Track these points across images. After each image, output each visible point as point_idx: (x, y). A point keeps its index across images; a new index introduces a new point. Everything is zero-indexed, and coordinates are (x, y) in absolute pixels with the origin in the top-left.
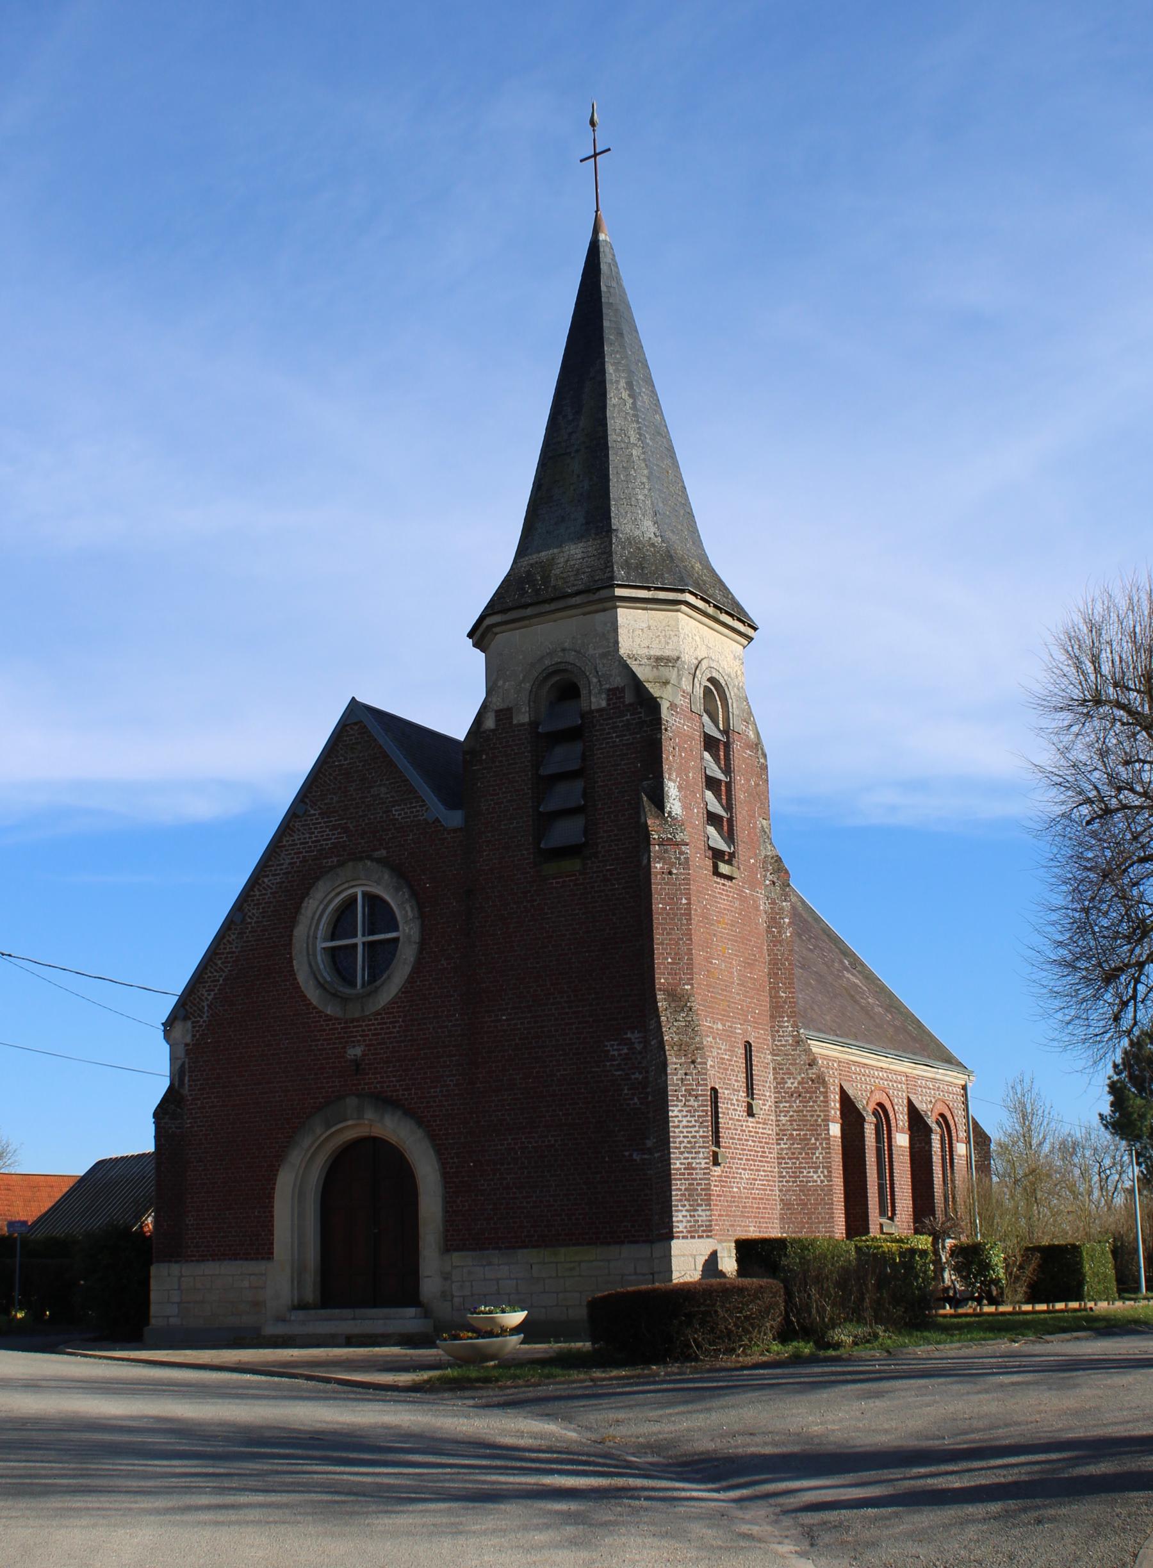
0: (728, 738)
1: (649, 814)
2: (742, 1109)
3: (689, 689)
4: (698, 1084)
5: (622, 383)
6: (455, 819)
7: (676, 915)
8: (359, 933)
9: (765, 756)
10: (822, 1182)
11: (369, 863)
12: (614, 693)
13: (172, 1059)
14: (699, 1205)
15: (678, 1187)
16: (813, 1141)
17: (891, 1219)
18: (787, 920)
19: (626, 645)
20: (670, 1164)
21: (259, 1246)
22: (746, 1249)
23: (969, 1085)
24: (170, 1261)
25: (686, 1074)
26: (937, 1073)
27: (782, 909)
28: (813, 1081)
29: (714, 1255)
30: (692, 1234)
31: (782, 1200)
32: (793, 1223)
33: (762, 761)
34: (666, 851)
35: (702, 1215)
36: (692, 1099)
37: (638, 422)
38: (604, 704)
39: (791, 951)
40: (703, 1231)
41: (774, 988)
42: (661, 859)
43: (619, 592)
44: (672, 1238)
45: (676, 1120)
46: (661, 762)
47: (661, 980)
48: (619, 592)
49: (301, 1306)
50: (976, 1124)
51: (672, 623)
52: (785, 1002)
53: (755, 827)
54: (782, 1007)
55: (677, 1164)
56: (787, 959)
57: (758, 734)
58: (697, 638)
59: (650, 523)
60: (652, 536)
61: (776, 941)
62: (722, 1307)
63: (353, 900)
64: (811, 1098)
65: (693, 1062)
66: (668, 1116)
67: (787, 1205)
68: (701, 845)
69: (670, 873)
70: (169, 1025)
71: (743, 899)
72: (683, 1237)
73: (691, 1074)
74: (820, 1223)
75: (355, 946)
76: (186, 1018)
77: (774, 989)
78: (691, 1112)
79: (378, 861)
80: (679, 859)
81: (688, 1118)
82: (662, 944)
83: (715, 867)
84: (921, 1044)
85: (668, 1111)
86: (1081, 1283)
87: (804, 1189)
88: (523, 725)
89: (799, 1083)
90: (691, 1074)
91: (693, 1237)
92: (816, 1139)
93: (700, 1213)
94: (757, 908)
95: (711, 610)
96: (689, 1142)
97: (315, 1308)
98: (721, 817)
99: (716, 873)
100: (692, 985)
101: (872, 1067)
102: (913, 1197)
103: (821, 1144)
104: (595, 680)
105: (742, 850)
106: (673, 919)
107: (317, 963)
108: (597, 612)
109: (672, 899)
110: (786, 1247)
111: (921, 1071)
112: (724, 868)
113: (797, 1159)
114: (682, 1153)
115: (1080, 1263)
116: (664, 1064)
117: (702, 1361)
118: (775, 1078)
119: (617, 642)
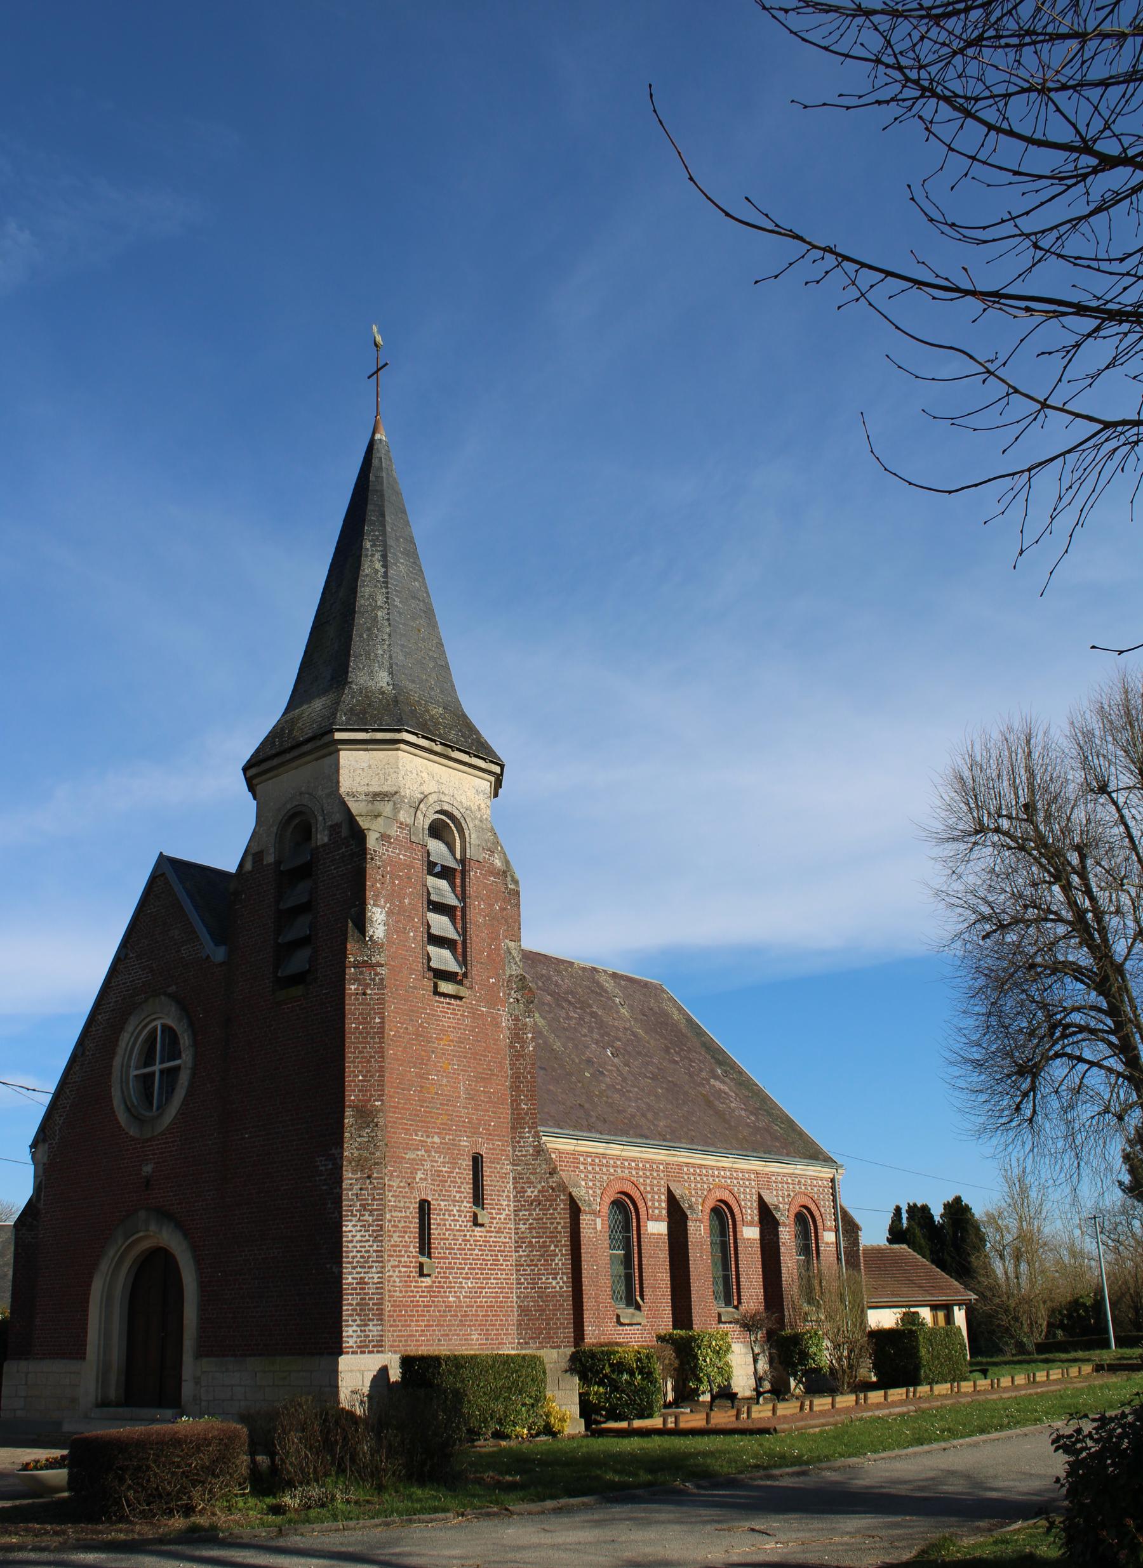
0: (464, 866)
1: (350, 939)
2: (465, 1221)
3: (410, 821)
4: (374, 1199)
5: (378, 556)
6: (219, 954)
7: (368, 1033)
9: (516, 882)
10: (561, 1288)
11: (163, 998)
12: (334, 829)
13: (35, 1177)
14: (370, 1320)
15: (350, 1301)
16: (552, 1248)
18: (530, 1035)
19: (347, 783)
21: (78, 1353)
22: (407, 1362)
23: (837, 1177)
24: (20, 1359)
25: (361, 1189)
27: (525, 1024)
28: (553, 1189)
29: (384, 1370)
30: (363, 1348)
31: (519, 1306)
32: (531, 1329)
33: (513, 887)
34: (361, 973)
35: (373, 1330)
36: (367, 1213)
37: (387, 588)
38: (326, 840)
39: (533, 1064)
40: (374, 1346)
43: (338, 736)
44: (341, 1353)
45: (350, 1234)
46: (365, 890)
47: (351, 1097)
48: (338, 736)
49: (103, 1404)
50: (845, 1214)
51: (392, 761)
52: (526, 1114)
53: (498, 948)
54: (523, 1118)
55: (349, 1279)
56: (529, 1073)
57: (507, 863)
58: (425, 775)
59: (386, 674)
60: (385, 685)
61: (518, 1056)
62: (155, 1461)
63: (155, 1029)
64: (551, 1206)
65: (369, 1177)
66: (341, 1232)
67: (524, 1311)
68: (419, 966)
69: (364, 994)
70: (34, 1145)
71: (474, 1014)
72: (353, 1353)
73: (367, 1189)
74: (558, 1328)
75: (153, 1074)
76: (44, 1141)
77: (516, 1102)
78: (365, 1226)
79: (169, 995)
80: (374, 980)
83: (436, 986)
84: (790, 1142)
85: (341, 1226)
86: (917, 1368)
87: (542, 1295)
88: (270, 865)
90: (367, 1189)
91: (363, 1352)
92: (556, 1246)
93: (371, 1327)
95: (438, 748)
96: (362, 1257)
97: (118, 1405)
98: (456, 941)
99: (436, 992)
100: (382, 1101)
102: (764, 1286)
104: (320, 818)
105: (475, 971)
106: (365, 1038)
107: (128, 1089)
108: (324, 756)
109: (365, 1020)
110: (440, 1364)
111: (772, 1167)
112: (446, 987)
113: (536, 1265)
115: (916, 1349)
116: (339, 1180)
117: (131, 1522)
118: (515, 1188)
119: (338, 782)
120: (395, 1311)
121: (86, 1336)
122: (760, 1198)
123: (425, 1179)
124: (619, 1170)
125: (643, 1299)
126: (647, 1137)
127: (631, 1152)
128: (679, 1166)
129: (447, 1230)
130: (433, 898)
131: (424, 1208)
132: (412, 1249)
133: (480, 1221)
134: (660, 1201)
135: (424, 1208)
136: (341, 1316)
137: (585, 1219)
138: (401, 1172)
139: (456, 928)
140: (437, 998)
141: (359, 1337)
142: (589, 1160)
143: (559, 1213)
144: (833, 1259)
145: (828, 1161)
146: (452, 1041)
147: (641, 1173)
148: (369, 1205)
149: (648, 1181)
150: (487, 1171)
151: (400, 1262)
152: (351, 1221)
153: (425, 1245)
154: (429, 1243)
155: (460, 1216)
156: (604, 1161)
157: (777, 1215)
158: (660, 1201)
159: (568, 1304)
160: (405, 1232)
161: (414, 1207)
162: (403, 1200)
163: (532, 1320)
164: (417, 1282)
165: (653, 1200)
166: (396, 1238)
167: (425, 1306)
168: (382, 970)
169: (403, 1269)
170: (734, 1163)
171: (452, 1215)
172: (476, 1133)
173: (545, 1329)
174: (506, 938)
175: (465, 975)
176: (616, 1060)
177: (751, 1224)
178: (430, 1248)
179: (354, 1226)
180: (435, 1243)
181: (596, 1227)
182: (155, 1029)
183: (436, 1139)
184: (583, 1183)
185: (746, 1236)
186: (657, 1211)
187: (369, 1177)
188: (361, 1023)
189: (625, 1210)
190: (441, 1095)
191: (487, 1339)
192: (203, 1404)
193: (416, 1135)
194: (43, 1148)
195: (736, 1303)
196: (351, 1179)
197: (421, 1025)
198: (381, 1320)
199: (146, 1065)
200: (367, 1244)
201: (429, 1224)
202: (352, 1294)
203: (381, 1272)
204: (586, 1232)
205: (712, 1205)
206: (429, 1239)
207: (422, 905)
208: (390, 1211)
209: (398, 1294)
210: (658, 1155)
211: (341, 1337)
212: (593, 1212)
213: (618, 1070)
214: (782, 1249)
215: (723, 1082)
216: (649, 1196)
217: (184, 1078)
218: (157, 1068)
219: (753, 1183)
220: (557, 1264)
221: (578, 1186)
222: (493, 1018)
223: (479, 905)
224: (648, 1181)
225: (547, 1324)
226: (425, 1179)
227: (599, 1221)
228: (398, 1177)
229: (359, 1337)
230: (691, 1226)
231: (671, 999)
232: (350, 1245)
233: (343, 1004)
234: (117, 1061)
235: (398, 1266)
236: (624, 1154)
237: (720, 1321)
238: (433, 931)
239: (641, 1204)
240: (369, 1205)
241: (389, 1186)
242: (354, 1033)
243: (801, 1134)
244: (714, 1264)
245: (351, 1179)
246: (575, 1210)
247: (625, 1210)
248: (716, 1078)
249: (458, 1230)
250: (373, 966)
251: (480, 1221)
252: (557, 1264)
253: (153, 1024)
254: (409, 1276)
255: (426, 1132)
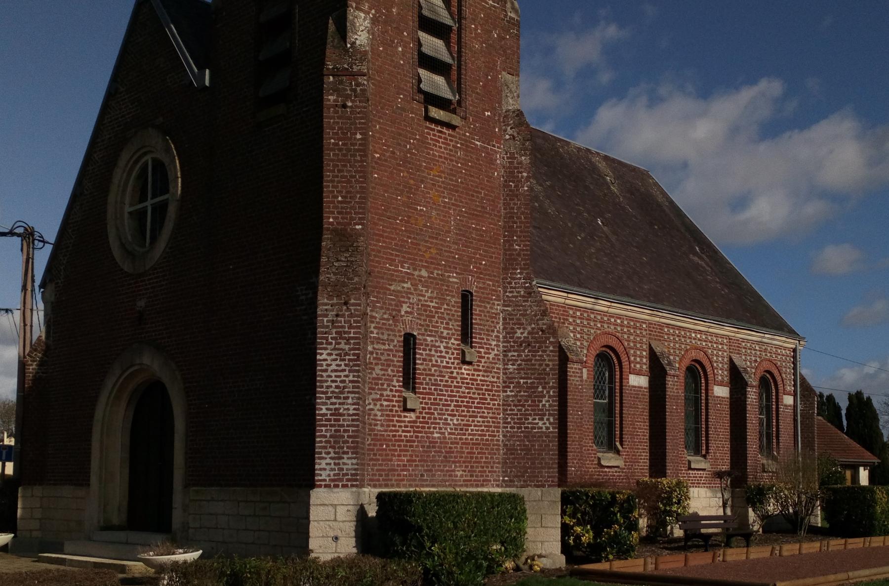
2: (451, 359)
4: (350, 327)
7: (349, 150)
8: (150, 196)
10: (547, 428)
14: (344, 453)
15: (323, 433)
16: (540, 389)
17: (704, 456)
18: (525, 174)
20: (315, 409)
21: (79, 477)
22: (381, 498)
25: (337, 316)
26: (764, 337)
27: (521, 163)
28: (542, 331)
30: (334, 484)
31: (505, 445)
32: (515, 467)
34: (341, 82)
36: (343, 342)
40: (348, 480)
41: (508, 241)
42: (336, 91)
44: (312, 485)
45: (324, 363)
49: (108, 527)
50: (803, 379)
52: (519, 255)
54: (516, 260)
56: (523, 213)
61: (513, 195)
63: (146, 164)
65: (346, 303)
67: (510, 450)
69: (344, 106)
71: (467, 146)
72: (326, 486)
74: (543, 468)
77: (509, 242)
78: (342, 355)
80: (355, 91)
81: (338, 362)
82: (332, 181)
84: (753, 311)
85: (316, 354)
87: (528, 435)
89: (528, 333)
91: (336, 486)
92: (544, 388)
93: (345, 461)
94: (492, 161)
96: (337, 387)
97: (120, 528)
99: (428, 118)
101: (690, 330)
103: (548, 392)
105: (470, 100)
111: (744, 335)
112: (435, 112)
113: (523, 406)
114: (329, 398)
118: (504, 328)
120: (375, 445)
121: (89, 464)
122: (731, 361)
123: (411, 313)
124: (606, 326)
125: (622, 445)
126: (632, 297)
127: (617, 309)
128: (661, 326)
129: (433, 366)
130: (425, 12)
131: (409, 343)
132: (395, 383)
133: (468, 359)
134: (641, 357)
135: (409, 343)
136: (314, 448)
137: (572, 368)
138: (384, 303)
139: (451, 54)
140: (428, 124)
141: (332, 470)
142: (578, 314)
143: (548, 355)
144: (790, 420)
145: (791, 333)
146: (443, 172)
147: (625, 330)
148: (345, 333)
149: (632, 338)
150: (476, 310)
151: (382, 395)
152: (326, 349)
153: (409, 379)
154: (414, 378)
155: (447, 353)
156: (592, 316)
157: (746, 377)
158: (641, 357)
159: (554, 445)
160: (389, 366)
161: (398, 341)
162: (386, 332)
163: (520, 461)
164: (400, 416)
165: (635, 356)
166: (378, 370)
167: (407, 441)
168: (362, 80)
169: (385, 403)
170: (710, 327)
171: (439, 351)
172: (466, 270)
173: (530, 468)
174: (504, 70)
175: (459, 103)
176: (605, 229)
177: (721, 384)
178: (414, 383)
179: (330, 354)
180: (420, 378)
181: (581, 376)
182: (146, 164)
183: (424, 273)
184: (572, 335)
185: (716, 394)
186: (638, 366)
187: (346, 303)
188: (340, 139)
189: (609, 361)
190: (431, 228)
191: (472, 476)
192: (191, 531)
193: (403, 267)
194: (51, 287)
195: (704, 452)
196: (326, 304)
197: (409, 151)
198: (356, 453)
199: (141, 201)
200: (342, 374)
201: (415, 359)
202: (326, 426)
203: (358, 404)
204: (573, 380)
205: (687, 365)
206: (414, 374)
207: (412, 21)
208: (372, 343)
209: (379, 428)
210: (643, 314)
211: (314, 470)
212: (581, 362)
213: (607, 237)
214: (749, 408)
215: (700, 258)
216: (632, 352)
217: (172, 210)
218: (149, 204)
219: (725, 348)
220: (544, 405)
221: (566, 336)
222: (488, 153)
223: (476, 29)
224: (632, 338)
225: (533, 463)
226: (411, 313)
227: (585, 370)
228: (381, 308)
229: (332, 470)
230: (670, 382)
231: (656, 184)
232: (324, 374)
233: (321, 117)
234: (112, 198)
235: (380, 400)
236: (611, 310)
237: (690, 468)
238: (424, 49)
239: (624, 358)
240: (345, 333)
241: (372, 317)
242: (333, 150)
243: (767, 308)
244: (687, 416)
245: (326, 304)
246: (563, 358)
247: (609, 361)
248: (695, 254)
249: (445, 367)
250: (354, 75)
251: (468, 359)
252: (544, 405)
253: (143, 160)
254: (391, 411)
255: (412, 264)
